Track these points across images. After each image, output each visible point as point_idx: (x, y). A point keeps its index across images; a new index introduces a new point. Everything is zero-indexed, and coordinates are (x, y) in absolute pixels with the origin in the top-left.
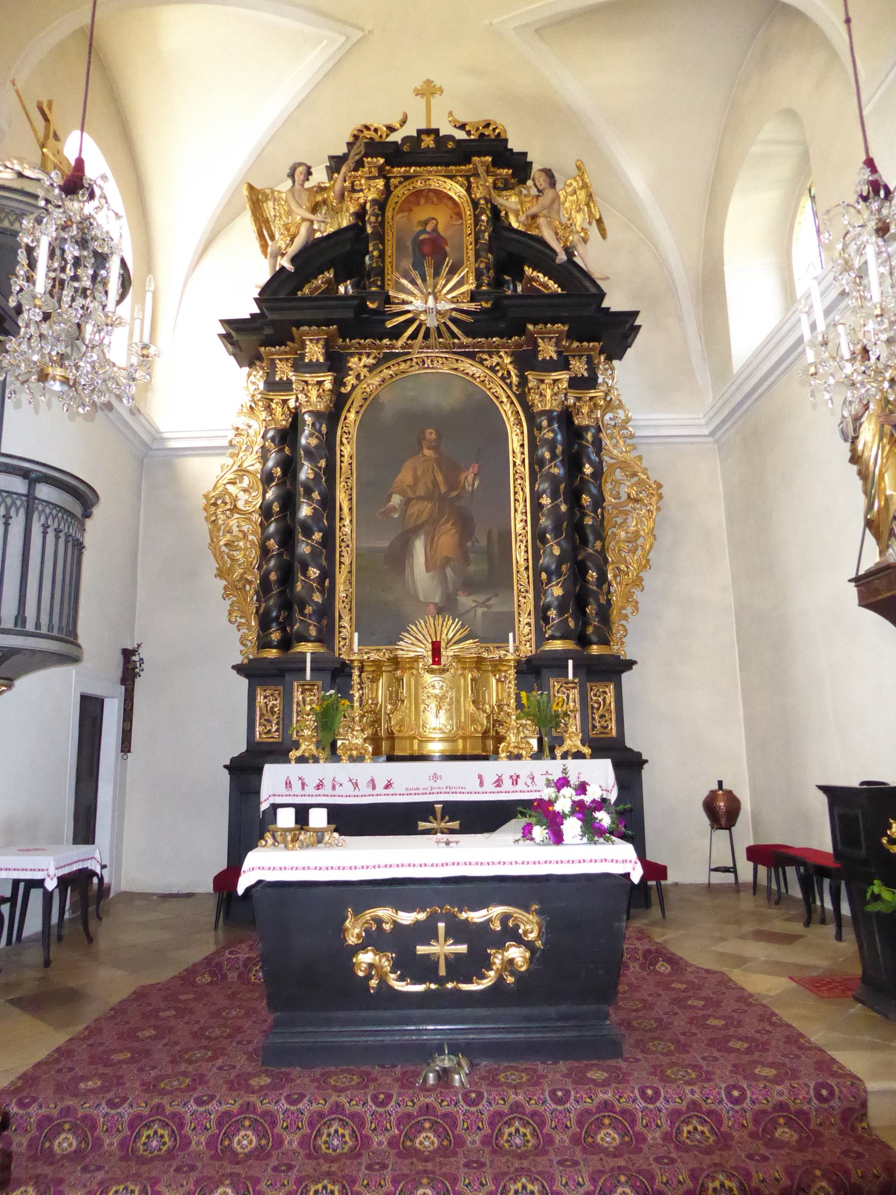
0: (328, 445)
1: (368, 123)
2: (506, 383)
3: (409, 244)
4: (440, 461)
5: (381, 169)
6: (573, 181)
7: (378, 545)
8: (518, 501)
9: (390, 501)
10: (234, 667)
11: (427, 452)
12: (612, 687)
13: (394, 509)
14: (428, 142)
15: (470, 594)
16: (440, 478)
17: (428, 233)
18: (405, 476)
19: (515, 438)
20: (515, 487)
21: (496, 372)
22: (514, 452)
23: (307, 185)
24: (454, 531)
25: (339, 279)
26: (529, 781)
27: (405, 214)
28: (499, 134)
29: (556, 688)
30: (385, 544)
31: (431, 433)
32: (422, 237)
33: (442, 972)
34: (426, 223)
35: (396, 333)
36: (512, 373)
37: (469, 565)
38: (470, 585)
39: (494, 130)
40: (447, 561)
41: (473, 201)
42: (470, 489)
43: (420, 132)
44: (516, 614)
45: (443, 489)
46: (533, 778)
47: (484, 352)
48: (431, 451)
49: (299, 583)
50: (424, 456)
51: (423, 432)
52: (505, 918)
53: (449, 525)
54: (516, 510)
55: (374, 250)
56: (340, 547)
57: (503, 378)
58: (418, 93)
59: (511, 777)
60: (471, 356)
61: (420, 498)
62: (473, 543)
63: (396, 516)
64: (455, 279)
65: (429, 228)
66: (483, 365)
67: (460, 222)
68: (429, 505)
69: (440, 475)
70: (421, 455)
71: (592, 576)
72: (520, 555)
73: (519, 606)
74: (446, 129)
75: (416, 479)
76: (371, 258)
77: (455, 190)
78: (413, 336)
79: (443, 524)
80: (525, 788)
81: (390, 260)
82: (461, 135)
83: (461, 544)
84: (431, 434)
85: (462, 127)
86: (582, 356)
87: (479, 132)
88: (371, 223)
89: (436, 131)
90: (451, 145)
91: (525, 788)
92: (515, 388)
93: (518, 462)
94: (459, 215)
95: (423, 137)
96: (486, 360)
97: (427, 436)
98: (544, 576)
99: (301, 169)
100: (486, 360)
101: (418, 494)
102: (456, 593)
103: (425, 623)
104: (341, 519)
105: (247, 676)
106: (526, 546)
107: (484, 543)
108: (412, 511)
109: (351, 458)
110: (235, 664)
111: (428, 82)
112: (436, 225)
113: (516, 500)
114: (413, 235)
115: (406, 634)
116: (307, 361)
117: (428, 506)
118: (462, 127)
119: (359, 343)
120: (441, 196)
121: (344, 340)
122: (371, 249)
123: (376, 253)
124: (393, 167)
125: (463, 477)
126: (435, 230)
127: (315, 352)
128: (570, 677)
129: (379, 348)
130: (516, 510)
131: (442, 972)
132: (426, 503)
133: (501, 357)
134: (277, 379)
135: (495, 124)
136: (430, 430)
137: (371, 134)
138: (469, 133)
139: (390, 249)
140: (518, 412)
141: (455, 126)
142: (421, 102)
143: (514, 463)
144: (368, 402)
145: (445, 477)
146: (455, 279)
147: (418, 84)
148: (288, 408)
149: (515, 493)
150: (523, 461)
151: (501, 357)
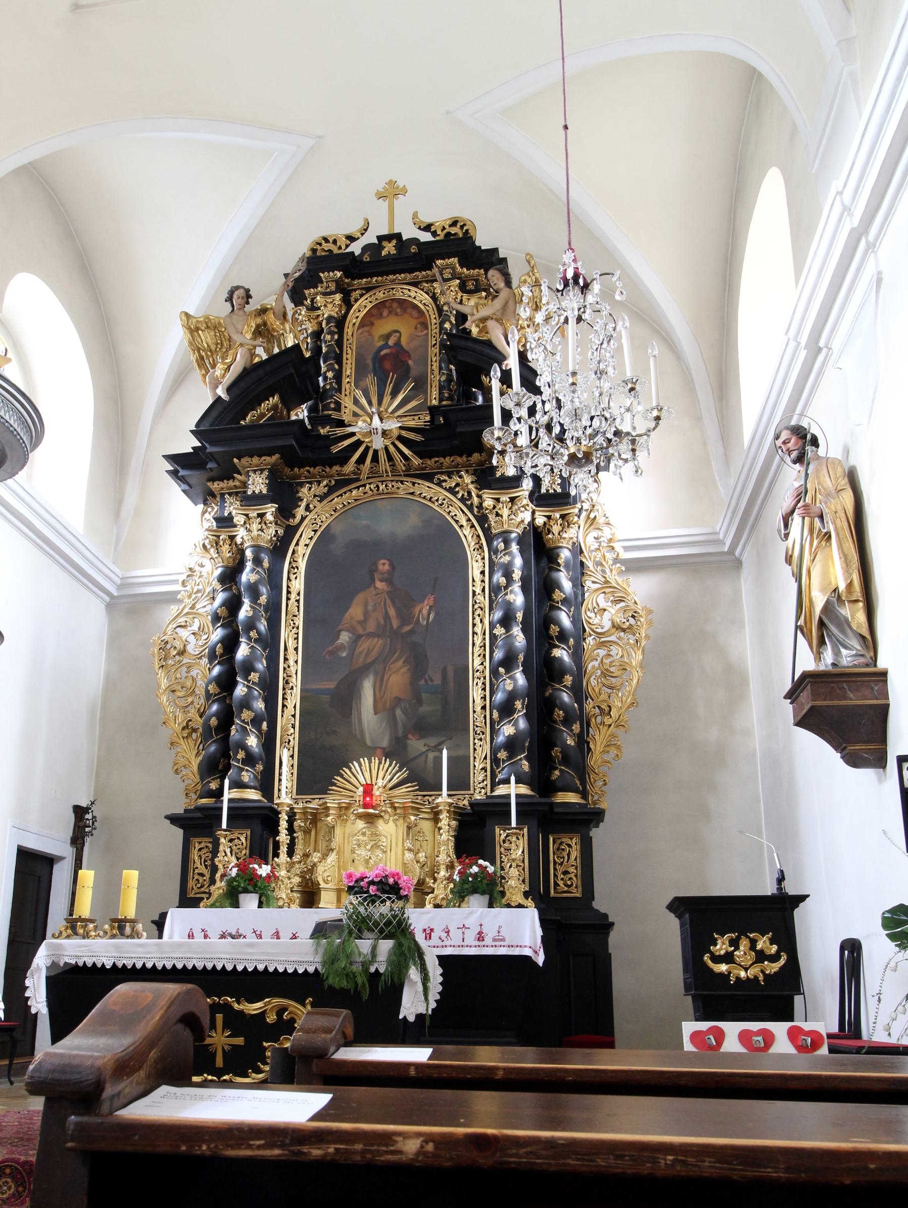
0: (274, 579)
1: (325, 234)
2: (466, 505)
3: (369, 362)
4: (394, 595)
5: (338, 282)
6: (527, 277)
7: (324, 687)
8: (477, 634)
9: (338, 638)
10: (167, 817)
11: (379, 585)
12: (526, 830)
13: (342, 647)
14: (389, 248)
15: (421, 737)
16: (392, 612)
17: (390, 347)
18: (355, 611)
19: (475, 565)
20: (474, 619)
21: (455, 494)
22: (473, 581)
23: (248, 308)
24: (405, 669)
25: (290, 403)
26: (444, 935)
27: (366, 329)
28: (467, 231)
29: (503, 837)
30: (333, 686)
31: (384, 564)
32: (383, 353)
33: (219, 1062)
34: (388, 336)
35: (343, 458)
36: (473, 494)
37: (421, 705)
38: (421, 728)
39: (462, 227)
40: (398, 701)
41: (437, 306)
42: (425, 622)
43: (381, 238)
44: (472, 759)
45: (395, 623)
46: (448, 932)
47: (442, 473)
48: (384, 584)
49: (234, 727)
50: (376, 588)
51: (375, 564)
52: (281, 1011)
53: (400, 663)
54: (474, 644)
55: (328, 370)
56: (284, 689)
57: (462, 500)
58: (381, 196)
59: (425, 930)
60: (429, 477)
61: (371, 635)
62: (426, 681)
63: (344, 654)
64: (400, 397)
65: (391, 342)
66: (442, 487)
67: (425, 332)
68: (380, 642)
69: (392, 608)
70: (372, 588)
71: (559, 715)
72: (476, 694)
73: (475, 750)
74: (409, 232)
75: (366, 614)
76: (325, 379)
77: (419, 297)
78: (361, 460)
79: (393, 663)
80: (440, 943)
81: (348, 380)
82: (426, 237)
83: (413, 683)
84: (384, 566)
85: (427, 228)
86: (264, 470)
87: (445, 231)
88: (326, 342)
89: (398, 236)
90: (414, 249)
91: (440, 943)
92: (476, 510)
93: (478, 590)
94: (425, 325)
95: (385, 243)
96: (445, 481)
97: (380, 567)
98: (496, 714)
99: (240, 292)
100: (445, 481)
101: (368, 631)
102: (406, 737)
103: (360, 765)
104: (286, 659)
105: (181, 827)
106: (484, 684)
107: (438, 681)
108: (361, 649)
109: (299, 594)
110: (169, 813)
111: (392, 183)
112: (400, 338)
113: (474, 633)
114: (374, 350)
115: (338, 778)
116: (249, 492)
117: (377, 644)
118: (427, 228)
119: (308, 471)
120: (406, 306)
121: (292, 470)
122: (323, 369)
123: (330, 374)
124: (353, 279)
125: (417, 609)
126: (398, 343)
127: (258, 484)
128: (514, 824)
129: (329, 476)
130: (474, 644)
131: (219, 1062)
132: (376, 639)
133: (461, 477)
134: (226, 514)
135: (463, 220)
136: (382, 561)
137: (330, 246)
138: (434, 234)
139: (349, 369)
140: (478, 536)
141: (419, 228)
142: (384, 205)
143: (474, 592)
144: (319, 533)
145: (398, 611)
146: (400, 397)
147: (380, 186)
148: (236, 544)
149: (474, 625)
150: (483, 590)
151: (461, 477)
